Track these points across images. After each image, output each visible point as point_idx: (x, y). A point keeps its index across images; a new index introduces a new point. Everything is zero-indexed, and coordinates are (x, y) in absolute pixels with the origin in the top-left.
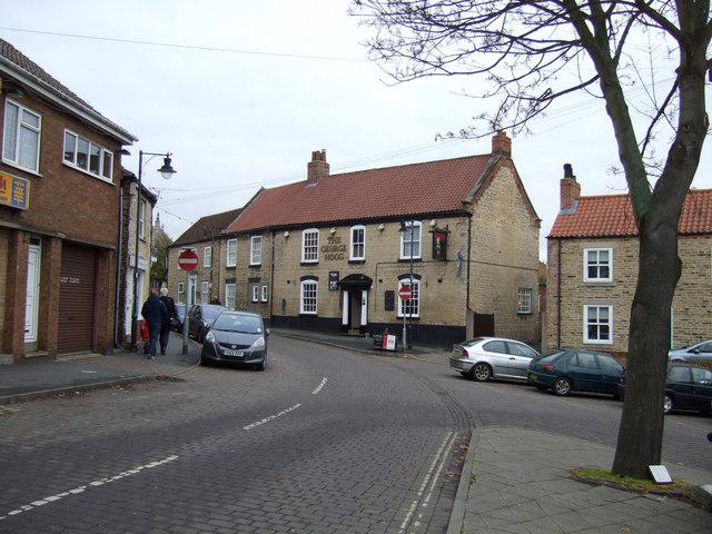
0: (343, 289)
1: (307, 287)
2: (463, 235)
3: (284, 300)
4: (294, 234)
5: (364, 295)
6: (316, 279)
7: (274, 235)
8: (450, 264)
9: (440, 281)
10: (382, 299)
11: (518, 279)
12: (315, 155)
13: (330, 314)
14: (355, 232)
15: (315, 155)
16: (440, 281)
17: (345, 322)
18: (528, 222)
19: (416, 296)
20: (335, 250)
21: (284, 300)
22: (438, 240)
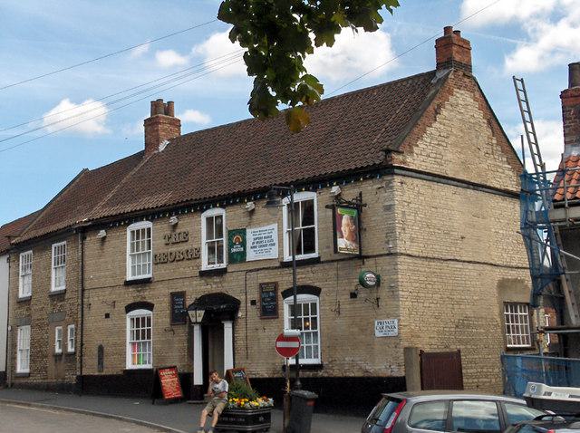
1: (137, 322)
3: (101, 349)
4: (114, 234)
5: (228, 327)
6: (150, 306)
7: (84, 238)
11: (503, 285)
12: (156, 105)
14: (209, 220)
15: (156, 105)
19: (314, 326)
21: (101, 349)
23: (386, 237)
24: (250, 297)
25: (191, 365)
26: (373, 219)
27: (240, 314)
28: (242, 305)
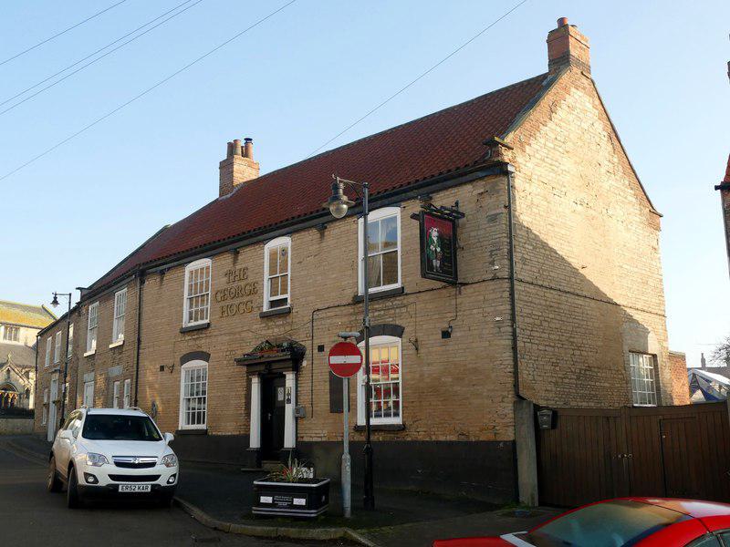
0: (250, 373)
2: (493, 218)
5: (290, 379)
6: (204, 356)
7: (142, 282)
8: (467, 290)
9: (446, 334)
10: (324, 389)
13: (229, 429)
16: (446, 334)
17: (255, 442)
18: (635, 214)
20: (237, 294)
22: (434, 233)
23: (491, 256)
24: (317, 342)
25: (248, 426)
26: (472, 234)
27: (305, 363)
28: (308, 352)
